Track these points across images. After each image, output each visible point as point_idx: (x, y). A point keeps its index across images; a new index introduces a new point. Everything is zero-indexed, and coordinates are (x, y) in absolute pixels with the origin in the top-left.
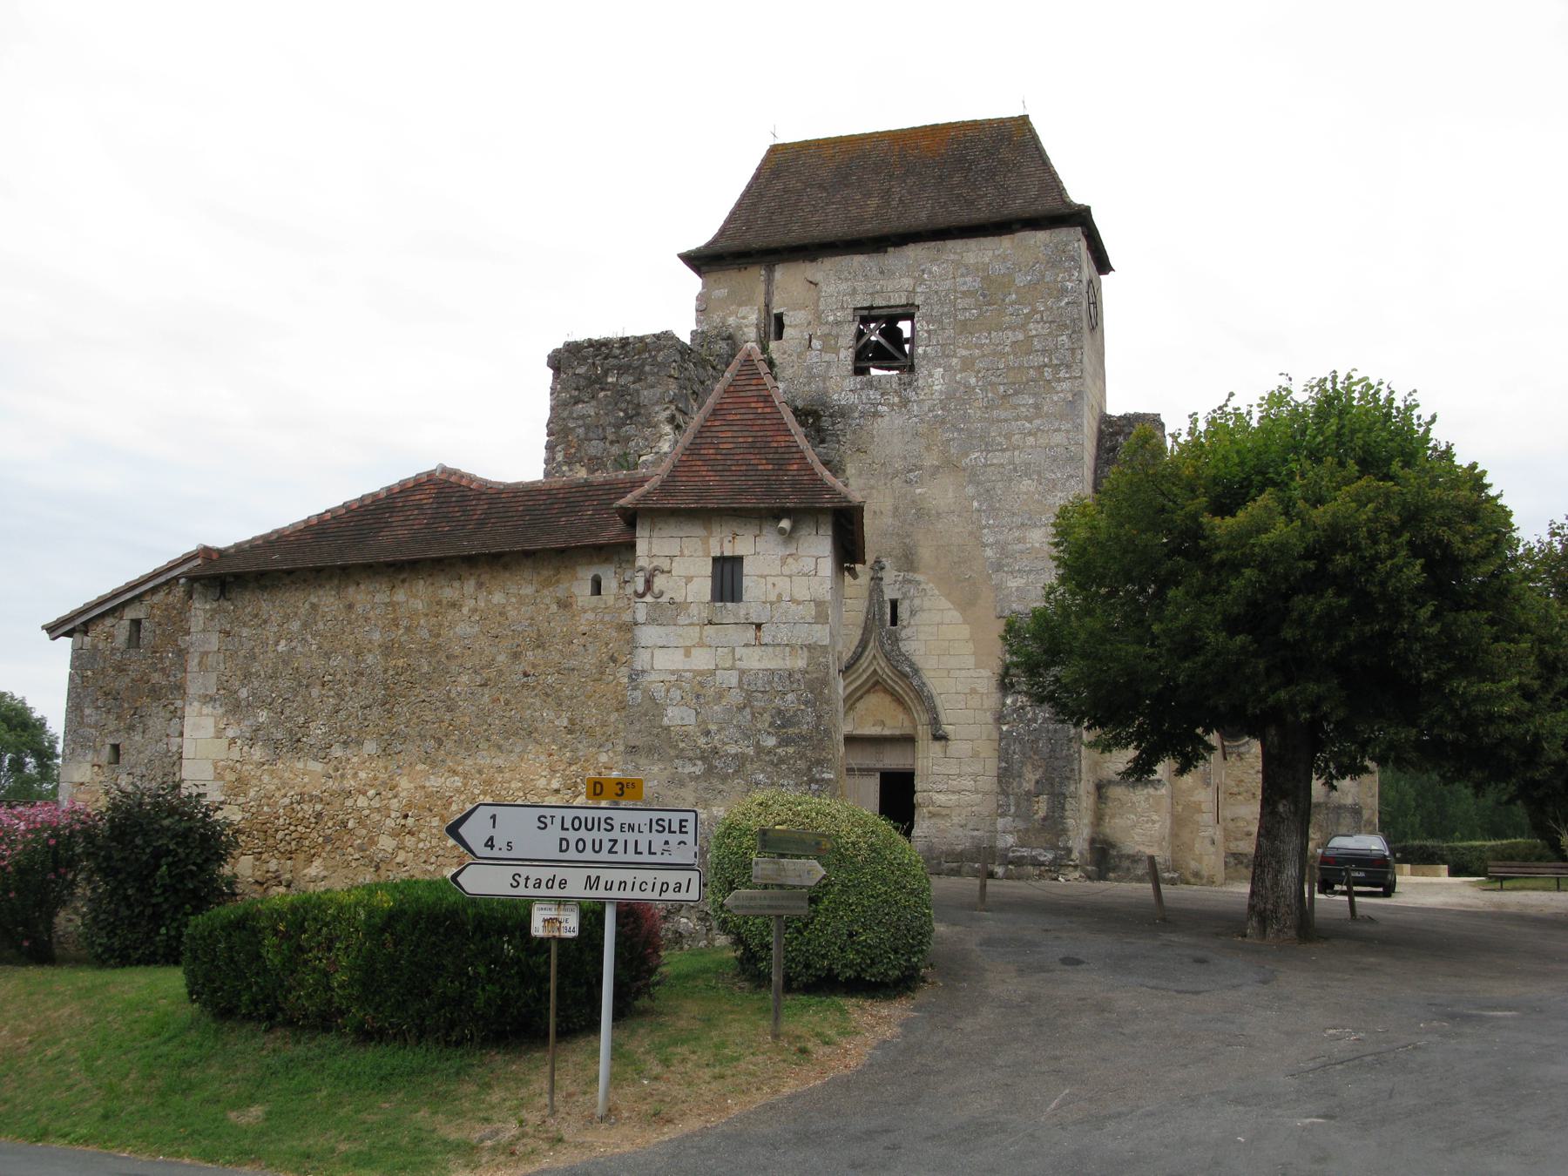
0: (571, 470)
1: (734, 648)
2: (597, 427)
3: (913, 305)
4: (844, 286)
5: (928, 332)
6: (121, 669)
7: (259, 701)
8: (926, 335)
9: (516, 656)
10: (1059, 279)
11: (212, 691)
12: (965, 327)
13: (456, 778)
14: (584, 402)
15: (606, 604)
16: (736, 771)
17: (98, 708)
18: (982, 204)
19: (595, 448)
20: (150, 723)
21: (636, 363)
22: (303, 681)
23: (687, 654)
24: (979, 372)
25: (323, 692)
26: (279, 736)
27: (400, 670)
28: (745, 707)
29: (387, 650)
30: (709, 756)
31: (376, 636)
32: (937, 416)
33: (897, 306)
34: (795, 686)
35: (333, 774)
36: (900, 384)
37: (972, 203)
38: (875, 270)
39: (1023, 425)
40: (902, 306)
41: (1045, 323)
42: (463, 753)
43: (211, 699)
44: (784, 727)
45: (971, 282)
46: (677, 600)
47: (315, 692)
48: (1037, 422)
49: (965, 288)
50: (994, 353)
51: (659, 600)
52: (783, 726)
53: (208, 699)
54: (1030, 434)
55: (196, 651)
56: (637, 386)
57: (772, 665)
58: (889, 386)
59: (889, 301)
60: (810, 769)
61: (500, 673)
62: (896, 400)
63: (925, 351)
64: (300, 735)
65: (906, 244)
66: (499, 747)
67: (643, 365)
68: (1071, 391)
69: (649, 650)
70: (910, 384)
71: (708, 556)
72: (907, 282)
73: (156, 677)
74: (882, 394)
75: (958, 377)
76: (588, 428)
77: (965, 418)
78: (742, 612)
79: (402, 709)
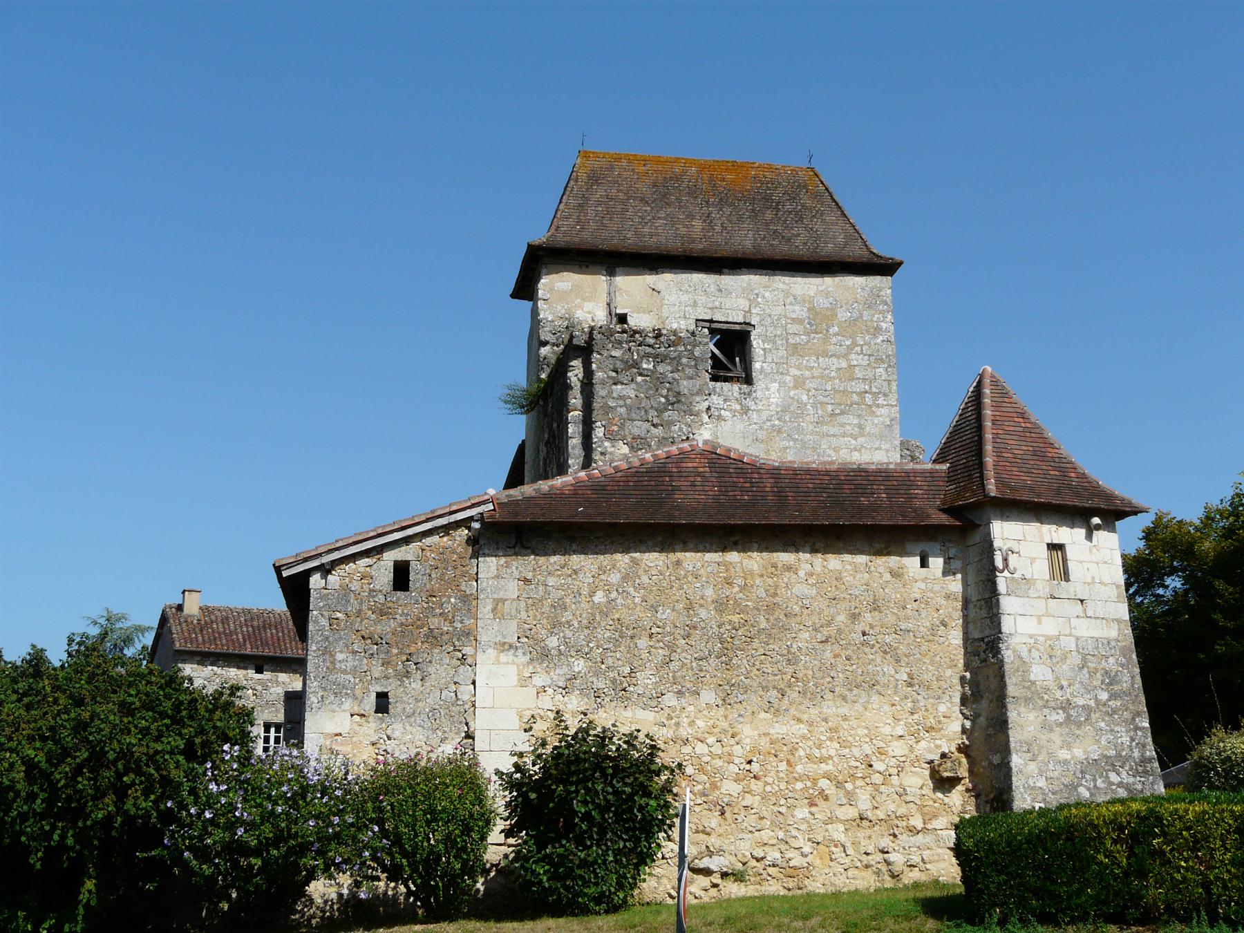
0: (613, 446)
1: (1069, 618)
2: (639, 408)
3: (749, 324)
4: (685, 298)
5: (764, 350)
6: (383, 612)
7: (571, 649)
8: (762, 352)
9: (854, 617)
10: (875, 319)
11: (513, 639)
12: (795, 349)
13: (802, 726)
14: (623, 384)
15: (934, 576)
16: (1087, 720)
17: (354, 652)
18: (798, 242)
19: (639, 428)
20: (432, 669)
21: (673, 355)
22: (625, 633)
23: (1039, 622)
24: (810, 391)
25: (651, 644)
26: (601, 685)
27: (737, 625)
28: (1083, 667)
29: (721, 606)
30: (1066, 706)
31: (709, 592)
32: (773, 426)
33: (736, 323)
34: (1113, 651)
35: (666, 722)
36: (740, 394)
37: (789, 240)
38: (713, 288)
39: (849, 441)
40: (740, 324)
41: (865, 355)
42: (807, 703)
43: (511, 646)
44: (1111, 684)
45: (799, 311)
46: (1028, 577)
47: (643, 643)
48: (860, 440)
49: (794, 316)
50: (822, 377)
51: (1014, 575)
52: (1111, 684)
53: (506, 647)
54: (855, 449)
55: (487, 597)
56: (676, 376)
57: (1097, 634)
58: (730, 393)
59: (728, 317)
60: (1133, 719)
61: (839, 631)
62: (738, 407)
63: (762, 367)
64: (625, 685)
65: (740, 269)
66: (844, 698)
67: (680, 357)
68: (889, 416)
69: (1012, 617)
70: (749, 394)
71: (1043, 542)
72: (744, 303)
73: (434, 622)
74: (725, 401)
75: (792, 393)
76: (629, 409)
77: (799, 430)
78: (1072, 590)
79: (740, 661)
